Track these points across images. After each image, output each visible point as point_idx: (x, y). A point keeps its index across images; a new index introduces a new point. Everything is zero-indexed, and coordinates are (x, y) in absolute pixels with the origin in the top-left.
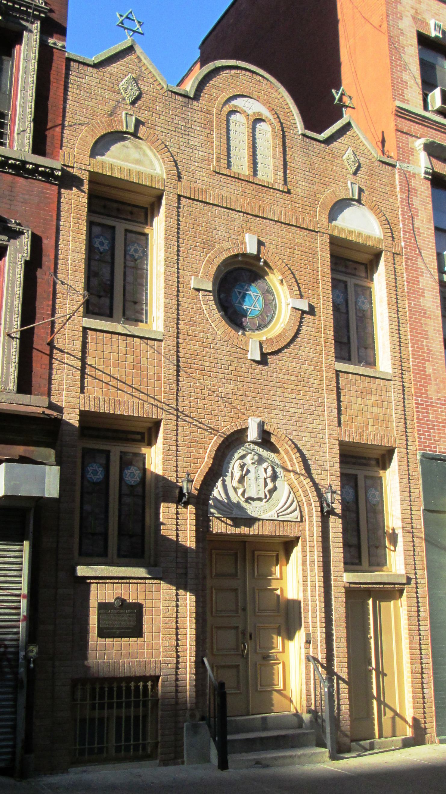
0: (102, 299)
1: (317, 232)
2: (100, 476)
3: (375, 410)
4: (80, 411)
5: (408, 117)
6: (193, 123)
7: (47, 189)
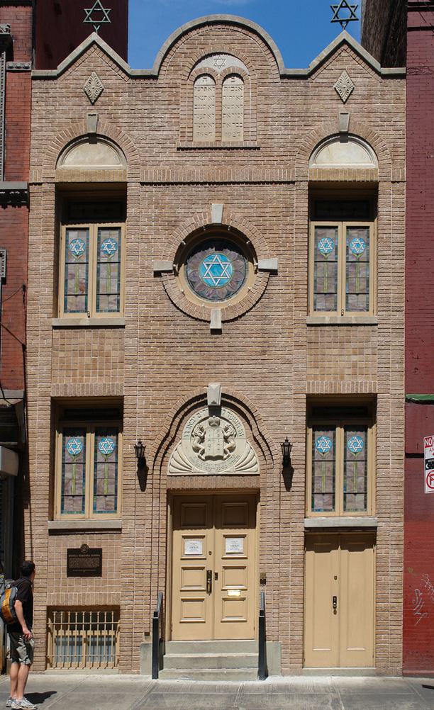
2: (79, 449)
3: (354, 358)
4: (52, 398)
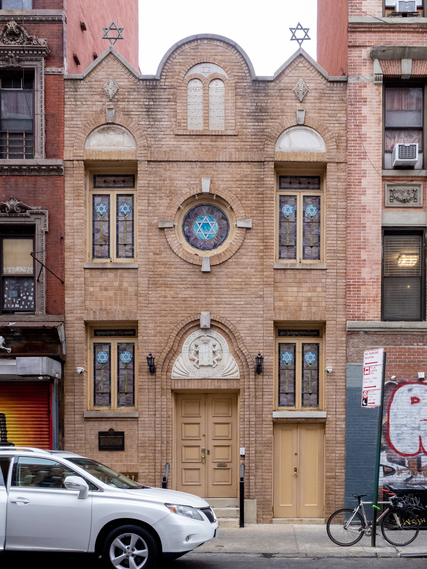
0: (103, 246)
1: (264, 162)
2: (106, 359)
5: (362, 30)
6: (159, 100)
7: (56, 180)
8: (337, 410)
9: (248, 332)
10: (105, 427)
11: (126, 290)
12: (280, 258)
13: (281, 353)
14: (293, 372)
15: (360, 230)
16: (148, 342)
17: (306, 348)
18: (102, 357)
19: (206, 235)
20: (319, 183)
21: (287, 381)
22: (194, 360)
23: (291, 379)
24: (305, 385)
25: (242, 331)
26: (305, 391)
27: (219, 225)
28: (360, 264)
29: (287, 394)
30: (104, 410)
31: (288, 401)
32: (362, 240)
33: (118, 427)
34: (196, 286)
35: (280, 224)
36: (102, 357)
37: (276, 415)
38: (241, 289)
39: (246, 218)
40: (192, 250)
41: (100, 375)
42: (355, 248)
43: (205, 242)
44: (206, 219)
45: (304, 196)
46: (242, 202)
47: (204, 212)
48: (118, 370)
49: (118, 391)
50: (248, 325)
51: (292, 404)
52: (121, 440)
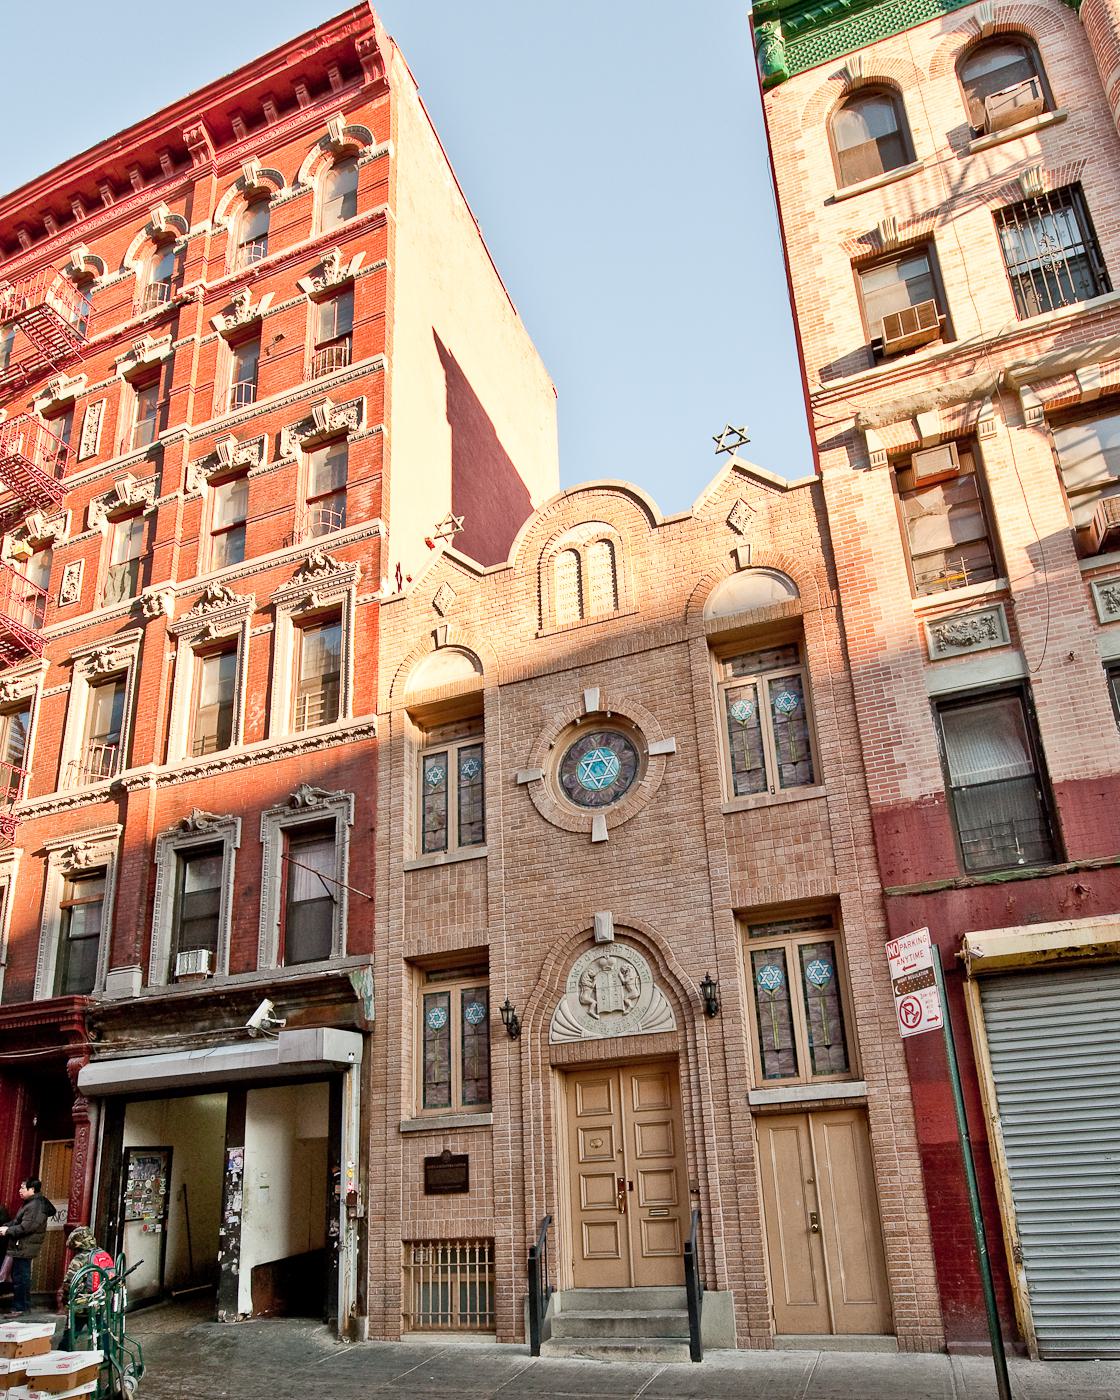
2: (442, 1021)
8: (890, 1076)
9: (685, 937)
10: (434, 1148)
11: (468, 897)
12: (736, 795)
13: (757, 969)
14: (785, 1005)
15: (884, 712)
16: (505, 985)
17: (807, 954)
18: (437, 1018)
19: (599, 781)
20: (797, 654)
21: (775, 1024)
22: (589, 1004)
23: (783, 1021)
24: (814, 1030)
25: (670, 943)
26: (816, 1043)
27: (620, 759)
28: (895, 773)
29: (778, 1051)
30: (440, 1117)
31: (783, 1066)
32: (891, 730)
33: (456, 1146)
34: (585, 870)
35: (731, 737)
36: (437, 1018)
37: (756, 1098)
38: (666, 862)
39: (667, 737)
40: (572, 809)
41: (433, 1051)
42: (880, 747)
43: (597, 792)
44: (598, 754)
45: (770, 681)
46: (656, 713)
47: (594, 744)
48: (463, 1037)
49: (463, 1077)
50: (683, 925)
51: (792, 1071)
52: (464, 1170)
